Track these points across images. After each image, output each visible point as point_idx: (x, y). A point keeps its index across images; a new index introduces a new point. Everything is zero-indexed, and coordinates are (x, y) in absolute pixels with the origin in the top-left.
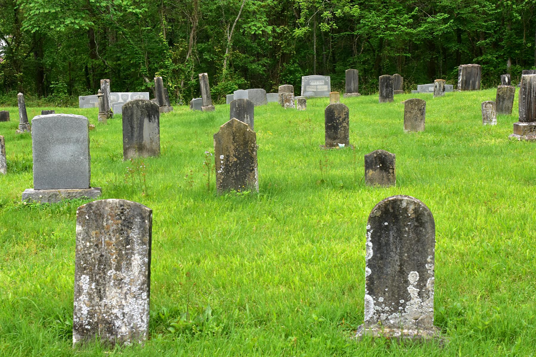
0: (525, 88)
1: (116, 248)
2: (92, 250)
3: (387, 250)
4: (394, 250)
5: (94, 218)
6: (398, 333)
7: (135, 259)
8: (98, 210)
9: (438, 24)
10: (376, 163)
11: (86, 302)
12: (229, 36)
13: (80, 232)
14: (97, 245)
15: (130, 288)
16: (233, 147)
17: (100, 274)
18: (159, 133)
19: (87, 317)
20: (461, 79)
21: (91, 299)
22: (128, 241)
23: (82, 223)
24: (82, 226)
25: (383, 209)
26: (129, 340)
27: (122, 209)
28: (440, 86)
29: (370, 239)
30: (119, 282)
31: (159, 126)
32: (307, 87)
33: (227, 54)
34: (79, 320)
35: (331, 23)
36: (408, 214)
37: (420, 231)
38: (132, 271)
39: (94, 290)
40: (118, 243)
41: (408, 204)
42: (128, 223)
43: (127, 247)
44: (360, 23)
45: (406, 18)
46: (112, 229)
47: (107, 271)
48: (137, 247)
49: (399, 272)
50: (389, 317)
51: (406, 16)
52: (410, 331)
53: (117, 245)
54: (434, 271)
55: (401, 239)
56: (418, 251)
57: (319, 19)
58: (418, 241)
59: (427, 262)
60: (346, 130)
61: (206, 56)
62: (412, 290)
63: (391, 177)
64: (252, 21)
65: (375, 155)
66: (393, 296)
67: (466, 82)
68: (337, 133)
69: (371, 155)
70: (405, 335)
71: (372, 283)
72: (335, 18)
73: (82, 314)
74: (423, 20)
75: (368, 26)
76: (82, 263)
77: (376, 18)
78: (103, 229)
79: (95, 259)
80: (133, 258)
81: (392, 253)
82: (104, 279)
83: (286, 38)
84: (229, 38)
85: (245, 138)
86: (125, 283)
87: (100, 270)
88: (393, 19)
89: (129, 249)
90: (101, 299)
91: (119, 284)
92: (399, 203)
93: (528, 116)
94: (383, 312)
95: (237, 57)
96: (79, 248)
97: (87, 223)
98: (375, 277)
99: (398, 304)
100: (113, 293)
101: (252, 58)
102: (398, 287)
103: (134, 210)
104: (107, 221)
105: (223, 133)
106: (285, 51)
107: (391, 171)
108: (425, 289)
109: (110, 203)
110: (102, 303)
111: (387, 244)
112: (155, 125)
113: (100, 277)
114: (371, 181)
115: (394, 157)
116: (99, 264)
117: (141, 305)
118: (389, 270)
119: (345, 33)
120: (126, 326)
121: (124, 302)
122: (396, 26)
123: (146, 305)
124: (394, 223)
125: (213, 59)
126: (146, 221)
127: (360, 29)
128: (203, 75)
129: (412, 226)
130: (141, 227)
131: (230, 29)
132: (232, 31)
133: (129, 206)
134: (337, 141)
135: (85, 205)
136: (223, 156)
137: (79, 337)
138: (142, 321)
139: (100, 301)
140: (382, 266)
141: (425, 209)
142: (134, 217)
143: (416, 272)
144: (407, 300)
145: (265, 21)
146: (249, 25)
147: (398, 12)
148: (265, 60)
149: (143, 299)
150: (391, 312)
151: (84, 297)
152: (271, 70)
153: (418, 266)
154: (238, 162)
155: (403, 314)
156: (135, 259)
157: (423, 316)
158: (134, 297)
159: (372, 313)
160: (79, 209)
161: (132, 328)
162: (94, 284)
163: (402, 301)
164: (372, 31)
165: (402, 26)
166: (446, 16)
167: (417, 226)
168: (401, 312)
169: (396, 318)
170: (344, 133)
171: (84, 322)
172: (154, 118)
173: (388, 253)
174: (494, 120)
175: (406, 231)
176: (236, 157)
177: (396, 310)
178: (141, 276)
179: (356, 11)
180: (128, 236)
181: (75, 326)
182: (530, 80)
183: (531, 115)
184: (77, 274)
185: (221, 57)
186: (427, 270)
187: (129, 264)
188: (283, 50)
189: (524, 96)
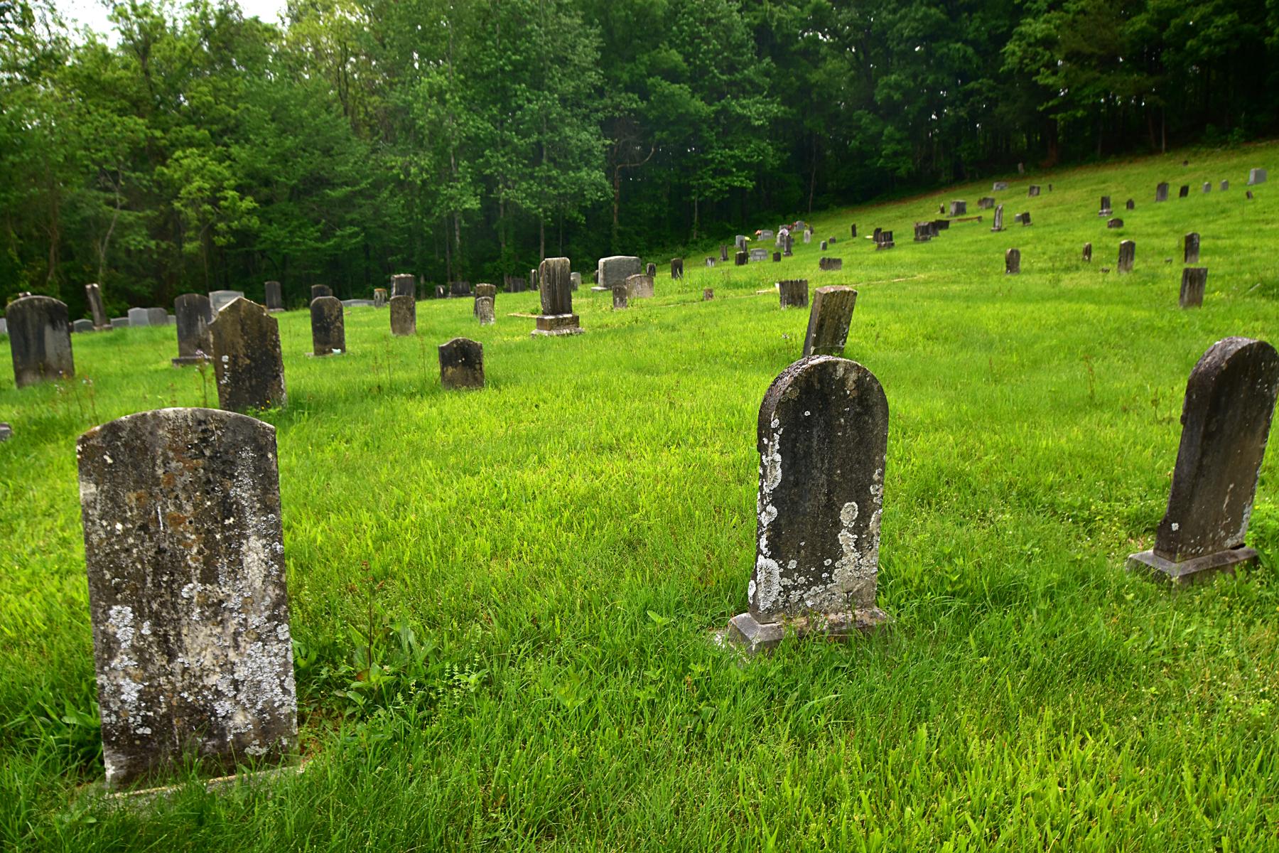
1: (197, 529)
2: (131, 540)
4: (819, 465)
5: (127, 459)
7: (250, 549)
8: (137, 438)
11: (131, 670)
12: (101, 253)
13: (92, 498)
14: (144, 527)
15: (245, 620)
16: (242, 343)
19: (138, 708)
22: (228, 507)
24: (97, 484)
26: (257, 742)
27: (204, 431)
29: (777, 447)
30: (215, 611)
34: (118, 717)
38: (245, 578)
41: (846, 370)
43: (227, 522)
45: (312, 231)
47: (180, 587)
48: (252, 520)
53: (198, 520)
57: (212, 230)
58: (860, 443)
60: (341, 332)
61: (74, 277)
62: (846, 538)
63: (478, 375)
66: (813, 554)
70: (836, 625)
73: (123, 702)
76: (108, 577)
78: (158, 485)
79: (142, 563)
80: (244, 548)
81: (815, 472)
82: (174, 608)
84: (102, 255)
85: (261, 327)
86: (232, 610)
89: (230, 527)
90: (172, 657)
91: (216, 614)
94: (795, 588)
96: (95, 538)
97: (110, 473)
98: (782, 522)
99: (821, 569)
100: (201, 638)
101: (133, 279)
103: (234, 432)
104: (166, 463)
109: (168, 419)
110: (177, 666)
111: (808, 454)
112: (64, 334)
113: (162, 605)
114: (449, 383)
115: (481, 347)
116: (155, 574)
117: (276, 655)
118: (808, 506)
120: (245, 709)
121: (232, 655)
123: (290, 655)
126: (270, 455)
127: (261, 243)
130: (258, 469)
131: (103, 244)
133: (222, 421)
135: (98, 428)
138: (285, 691)
139: (169, 662)
140: (796, 499)
141: (874, 379)
142: (237, 447)
144: (835, 559)
148: (149, 280)
149: (281, 641)
151: (123, 661)
156: (250, 549)
157: (862, 583)
158: (259, 639)
159: (776, 593)
160: (82, 442)
161: (261, 711)
162: (147, 624)
163: (828, 562)
168: (826, 584)
171: (131, 720)
173: (808, 472)
176: (249, 357)
177: (818, 580)
178: (271, 588)
180: (227, 496)
187: (237, 564)
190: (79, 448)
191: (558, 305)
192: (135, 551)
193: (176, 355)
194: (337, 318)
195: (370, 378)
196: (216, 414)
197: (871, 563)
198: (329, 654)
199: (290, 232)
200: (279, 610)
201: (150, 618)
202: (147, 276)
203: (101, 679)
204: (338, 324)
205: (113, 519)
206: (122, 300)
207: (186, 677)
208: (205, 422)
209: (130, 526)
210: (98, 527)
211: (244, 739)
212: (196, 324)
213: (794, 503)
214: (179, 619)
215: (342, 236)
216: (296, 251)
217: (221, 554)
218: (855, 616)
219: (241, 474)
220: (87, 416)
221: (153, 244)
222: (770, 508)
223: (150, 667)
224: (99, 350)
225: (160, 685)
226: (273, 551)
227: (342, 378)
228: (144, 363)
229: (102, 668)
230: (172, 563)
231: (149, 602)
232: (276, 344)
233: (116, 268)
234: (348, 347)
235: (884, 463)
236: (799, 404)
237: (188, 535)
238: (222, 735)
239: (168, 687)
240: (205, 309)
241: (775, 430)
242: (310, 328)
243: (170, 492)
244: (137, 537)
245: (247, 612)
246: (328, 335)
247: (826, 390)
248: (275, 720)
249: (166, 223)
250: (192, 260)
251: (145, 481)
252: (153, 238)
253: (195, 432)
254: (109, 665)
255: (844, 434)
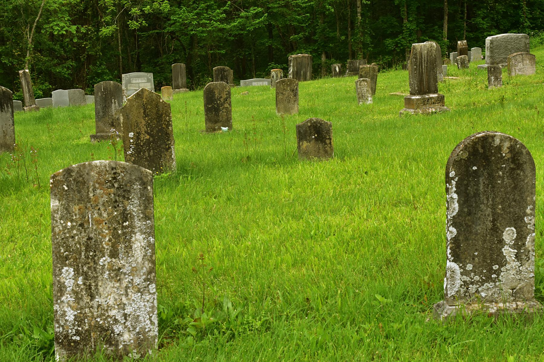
0: (416, 58)
1: (109, 227)
2: (75, 232)
3: (476, 202)
4: (485, 202)
5: (75, 188)
6: (492, 308)
8: (81, 176)
9: (252, 18)
10: (311, 133)
12: (29, 38)
13: (56, 208)
15: (132, 280)
16: (144, 123)
17: (89, 263)
18: (13, 125)
20: (291, 70)
21: (78, 299)
22: (125, 216)
23: (58, 196)
24: (59, 201)
25: (471, 149)
26: (135, 351)
27: (115, 173)
28: (277, 76)
29: (454, 189)
30: (117, 274)
31: (13, 117)
32: (129, 85)
33: (28, 57)
34: (63, 329)
35: (140, 20)
36: (501, 154)
37: (517, 175)
38: (133, 256)
39: (82, 287)
40: (112, 219)
41: (501, 140)
42: (124, 191)
43: (125, 224)
44: (169, 20)
46: (101, 201)
48: (138, 223)
49: (491, 229)
50: (480, 289)
51: (218, 11)
52: (507, 304)
54: (534, 225)
55: (493, 187)
56: (515, 201)
57: (126, 15)
58: (515, 188)
59: (526, 214)
60: (229, 111)
62: (508, 252)
63: (328, 148)
64: (54, 21)
65: (309, 124)
66: (484, 261)
67: (297, 73)
68: (218, 116)
69: (304, 124)
71: (458, 247)
72: (144, 15)
73: (66, 321)
74: (236, 15)
75: (179, 22)
76: (62, 251)
77: (187, 14)
78: (90, 202)
79: (80, 244)
80: (133, 239)
81: (482, 206)
82: (95, 270)
83: (91, 39)
84: (30, 40)
85: (158, 110)
86: (125, 274)
87: (88, 258)
88: (205, 15)
89: (126, 227)
90: (92, 297)
91: (117, 276)
92: (490, 140)
93: (421, 89)
94: (472, 283)
95: (39, 61)
96: (57, 230)
97: (66, 195)
98: (461, 238)
100: (108, 288)
101: (56, 61)
102: (491, 249)
103: (130, 174)
104: (94, 190)
105: (131, 106)
106: (90, 53)
107: (328, 141)
108: (524, 249)
109: (97, 167)
110: (95, 303)
111: (476, 194)
112: (9, 115)
113: (89, 268)
114: (305, 154)
115: (331, 126)
116: (86, 251)
117: (148, 301)
118: (479, 228)
119: (153, 31)
120: (129, 331)
122: (208, 22)
123: (155, 302)
124: (484, 166)
125: (12, 63)
126: (149, 188)
127: (170, 25)
128: (24, 72)
129: (507, 170)
130: (142, 195)
132: (32, 32)
133: (124, 168)
134: (219, 124)
135: (61, 171)
136: (132, 133)
137: (65, 353)
138: (152, 323)
139: (91, 300)
140: (470, 224)
141: (523, 146)
142: (131, 182)
143: (513, 228)
144: (501, 265)
145: (68, 20)
146: (51, 25)
147: (209, 7)
148: (71, 63)
149: (150, 294)
150: (483, 282)
151: (68, 298)
152: (77, 70)
153: (515, 221)
154: (151, 139)
155: (497, 284)
156: (136, 240)
157: (523, 284)
158: (139, 291)
159: (458, 286)
160: (53, 178)
161: (138, 333)
162: (81, 278)
163: (495, 267)
164: (183, 28)
165: (215, 21)
166: (260, 9)
167: (513, 169)
168: (494, 282)
169: (488, 289)
170: (226, 115)
171: (70, 331)
172: (7, 106)
173: (478, 206)
174: (369, 99)
175: (499, 176)
176: (148, 134)
177: (489, 279)
178: (146, 263)
179: (166, 7)
180: (125, 210)
181: (57, 338)
182: (421, 49)
183: (424, 87)
184: (56, 267)
185: (21, 61)
186: (526, 225)
187: (129, 248)
188: (88, 52)
189: (415, 67)
190: (51, 181)
191: (425, 84)
192: (76, 238)
193: (94, 132)
194: (226, 100)
195: (242, 151)
196: (121, 164)
197: (529, 270)
198: (181, 312)
199: (197, 14)
200: (151, 276)
201: (82, 275)
202: (68, 59)
203: (56, 307)
204: (226, 105)
205: (66, 220)
206: (50, 80)
207: (100, 310)
208: (115, 168)
209: (75, 224)
210: (58, 224)
211: (128, 348)
212: (110, 106)
213: (468, 226)
214: (97, 277)
215: (247, 18)
216: (203, 32)
217: (121, 240)
218: (517, 306)
219: (133, 197)
220: (30, 178)
221: (73, 28)
222: (452, 229)
223: (81, 302)
224: (30, 128)
225: (85, 313)
226: (149, 242)
227: (223, 151)
228: (68, 139)
229: (57, 301)
230: (96, 245)
231: (82, 266)
232: (169, 124)
233: (40, 51)
234: (236, 125)
235: (534, 202)
236: (469, 162)
237: (104, 230)
238: (117, 345)
239: (90, 314)
240: (117, 93)
241: (453, 179)
242: (202, 108)
243: (96, 206)
244: (78, 230)
245: (133, 276)
246: (217, 113)
247: (488, 154)
248: (146, 339)
249: (86, 9)
250: (107, 41)
251: (84, 200)
252: (74, 23)
253: (110, 174)
254: (60, 299)
255: (503, 182)
